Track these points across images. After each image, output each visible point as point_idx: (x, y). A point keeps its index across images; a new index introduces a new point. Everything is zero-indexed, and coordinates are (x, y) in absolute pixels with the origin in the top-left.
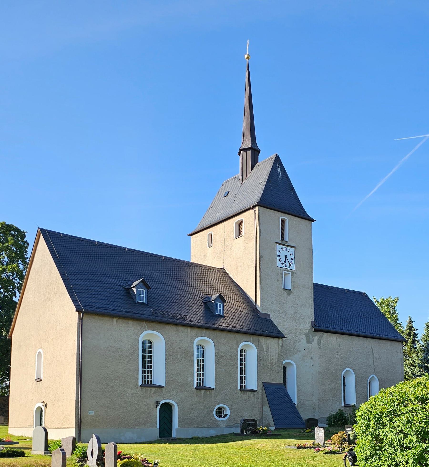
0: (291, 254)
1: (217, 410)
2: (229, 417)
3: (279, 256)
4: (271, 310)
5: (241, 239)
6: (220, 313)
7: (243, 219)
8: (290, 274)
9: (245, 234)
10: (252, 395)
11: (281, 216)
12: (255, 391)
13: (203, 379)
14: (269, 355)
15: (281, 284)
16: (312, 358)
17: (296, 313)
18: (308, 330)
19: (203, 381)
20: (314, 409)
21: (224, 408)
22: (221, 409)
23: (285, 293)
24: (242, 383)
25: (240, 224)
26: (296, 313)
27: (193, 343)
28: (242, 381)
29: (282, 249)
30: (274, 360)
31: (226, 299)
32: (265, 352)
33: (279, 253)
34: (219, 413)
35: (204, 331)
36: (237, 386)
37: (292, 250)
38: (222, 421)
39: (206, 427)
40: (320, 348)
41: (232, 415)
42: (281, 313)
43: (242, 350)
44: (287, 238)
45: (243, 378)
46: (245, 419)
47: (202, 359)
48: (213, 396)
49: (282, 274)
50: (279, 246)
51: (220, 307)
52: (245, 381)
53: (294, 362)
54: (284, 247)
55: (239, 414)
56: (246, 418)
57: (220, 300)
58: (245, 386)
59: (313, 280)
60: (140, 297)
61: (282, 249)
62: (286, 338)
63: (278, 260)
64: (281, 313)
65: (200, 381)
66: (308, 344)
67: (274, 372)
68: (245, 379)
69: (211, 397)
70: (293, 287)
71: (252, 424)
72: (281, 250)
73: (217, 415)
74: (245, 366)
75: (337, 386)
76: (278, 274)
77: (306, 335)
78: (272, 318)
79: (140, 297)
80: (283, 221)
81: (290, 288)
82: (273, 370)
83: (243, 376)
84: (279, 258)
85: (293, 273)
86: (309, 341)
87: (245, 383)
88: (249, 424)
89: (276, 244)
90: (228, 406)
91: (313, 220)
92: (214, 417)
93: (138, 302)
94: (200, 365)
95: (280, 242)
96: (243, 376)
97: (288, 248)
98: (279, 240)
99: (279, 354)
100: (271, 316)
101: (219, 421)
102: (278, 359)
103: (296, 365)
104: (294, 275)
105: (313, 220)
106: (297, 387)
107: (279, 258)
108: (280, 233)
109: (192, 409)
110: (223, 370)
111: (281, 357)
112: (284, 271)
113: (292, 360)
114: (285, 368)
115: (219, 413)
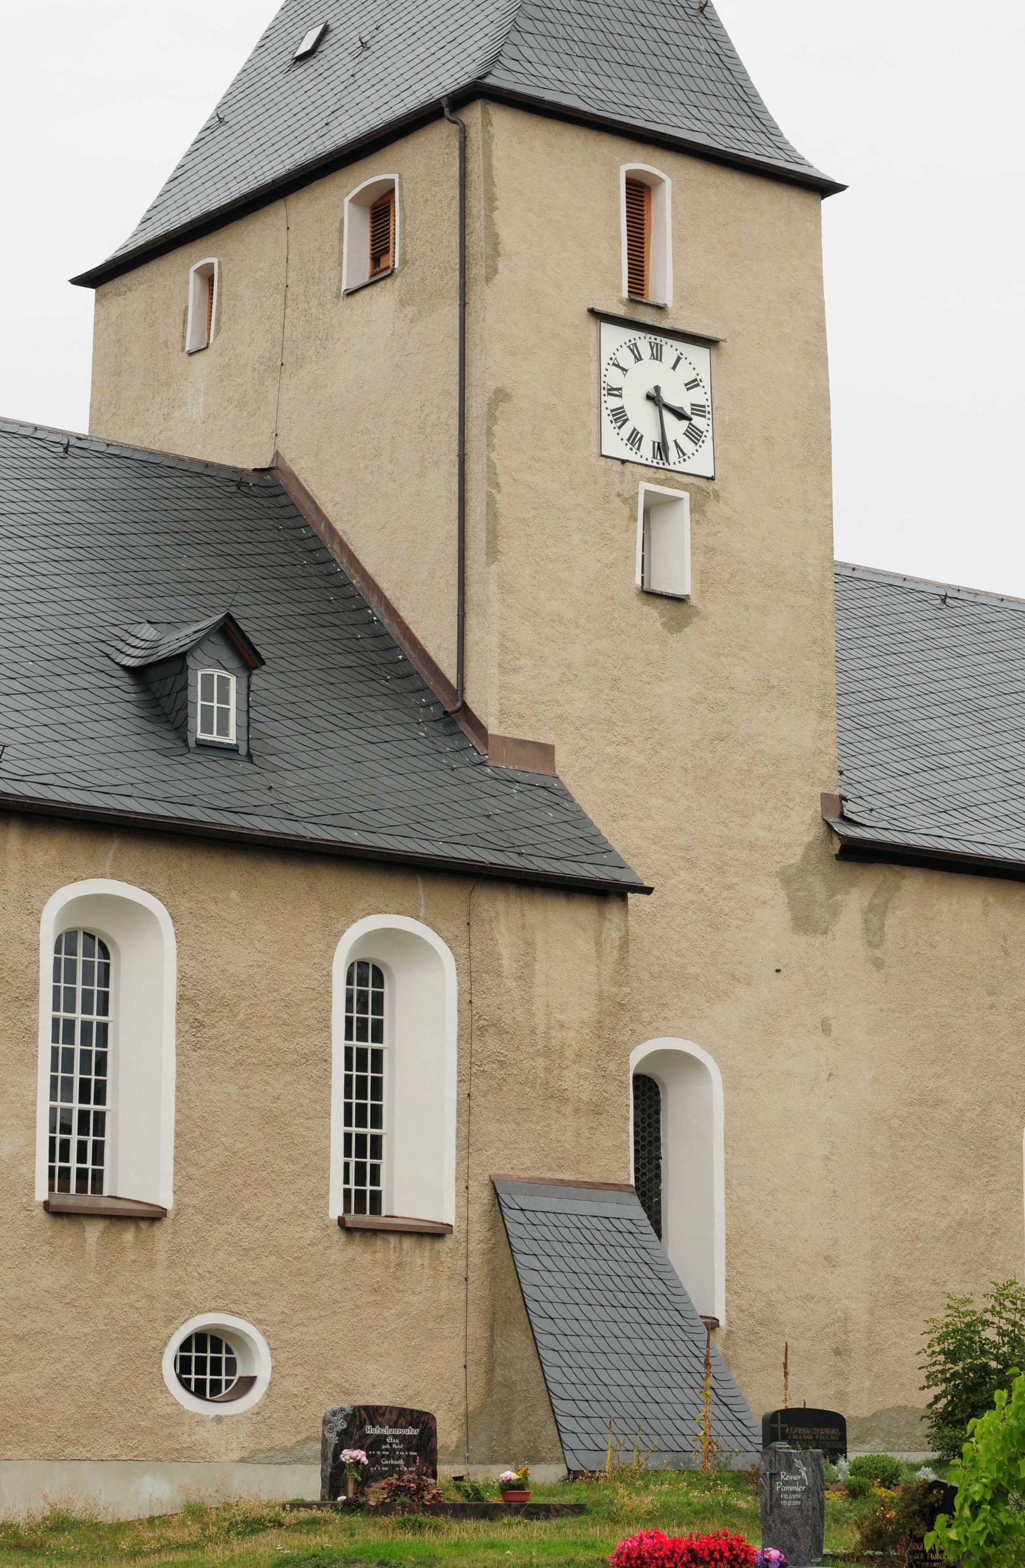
0: (692, 384)
1: (185, 1346)
2: (268, 1395)
3: (615, 392)
4: (562, 718)
5: (382, 299)
6: (223, 730)
7: (395, 177)
8: (686, 506)
9: (404, 262)
10: (418, 1256)
11: (625, 161)
12: (436, 1233)
13: (99, 1147)
14: (539, 1004)
15: (628, 558)
16: (826, 1028)
17: (720, 738)
18: (799, 851)
19: (98, 1159)
20: (837, 1352)
21: (239, 1337)
22: (217, 1347)
23: (653, 614)
24: (360, 1180)
25: (380, 209)
26: (720, 738)
27: (35, 915)
28: (360, 1167)
29: (634, 349)
30: (571, 1036)
31: (264, 654)
32: (510, 983)
33: (613, 378)
34: (201, 1370)
35: (111, 851)
36: (324, 1196)
37: (698, 357)
38: (219, 1419)
39: (115, 1458)
40: (878, 964)
41: (289, 1385)
42: (628, 740)
43: (362, 965)
44: (663, 286)
45: (365, 1150)
46: (357, 1409)
47: (95, 1018)
48: (161, 1257)
49: (630, 500)
50: (614, 337)
51: (224, 698)
52: (375, 1169)
53: (712, 1050)
54: (644, 342)
55: (334, 1375)
56: (361, 1401)
57: (224, 654)
58: (376, 1196)
59: (827, 540)
60: (207, 711)
61: (634, 349)
62: (648, 891)
63: (606, 419)
64: (628, 740)
65: (82, 1158)
66: (802, 940)
67: (568, 1109)
68: (377, 1153)
69: (151, 1265)
70: (703, 576)
71: (403, 1438)
72: (626, 358)
73: (185, 1384)
74: (378, 1067)
75: (989, 1206)
76: (606, 499)
77: (789, 878)
78: (567, 767)
79: (207, 711)
80: (639, 191)
81: (683, 587)
82: (561, 1097)
83: (369, 1131)
84: (613, 403)
85: (704, 489)
86: (805, 921)
87: (375, 1181)
88: (381, 1439)
89: (592, 324)
90: (257, 1322)
91: (825, 188)
92: (165, 1391)
93: (202, 745)
94: (86, 1055)
95: (620, 311)
96: (369, 1131)
97: (671, 348)
98: (615, 299)
99: (601, 996)
100: (561, 758)
101: (200, 1421)
102: (600, 1025)
103: (726, 1069)
104: (711, 507)
105: (825, 188)
106: (728, 1208)
107: (613, 403)
108: (617, 254)
109: (21, 1339)
110: (233, 1089)
111: (615, 1016)
112: (644, 486)
113: (696, 1039)
114: (647, 1091)
115: (201, 1370)
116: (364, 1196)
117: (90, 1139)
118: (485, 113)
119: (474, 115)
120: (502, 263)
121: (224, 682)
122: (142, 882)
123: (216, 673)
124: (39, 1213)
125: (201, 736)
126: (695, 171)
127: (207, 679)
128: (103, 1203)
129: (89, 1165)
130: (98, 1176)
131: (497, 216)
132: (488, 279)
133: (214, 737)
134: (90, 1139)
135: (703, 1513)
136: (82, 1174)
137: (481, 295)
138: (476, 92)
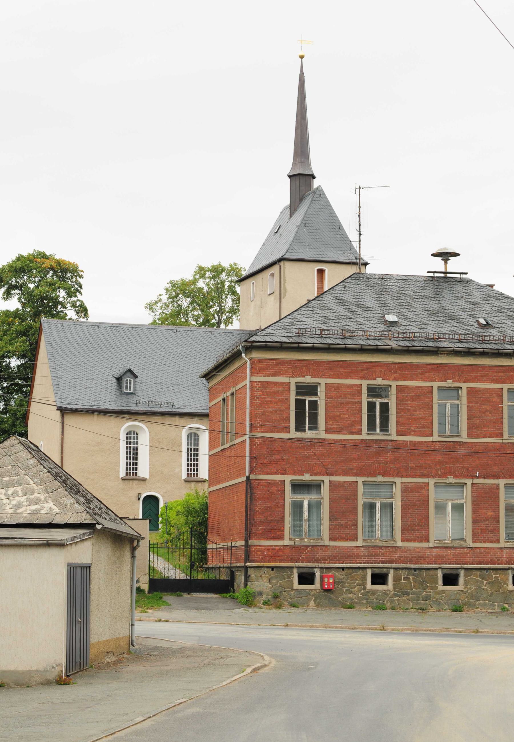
35: (195, 420)
93: (125, 393)
116: (132, 466)
117: (196, 468)
118: (284, 263)
119: (282, 263)
120: (287, 294)
121: (130, 381)
122: (139, 421)
123: (129, 379)
124: (183, 481)
125: (125, 391)
126: (333, 266)
127: (127, 380)
128: (137, 477)
129: (195, 472)
130: (197, 474)
131: (286, 284)
132: (284, 297)
133: (128, 391)
134: (196, 468)
135: (317, 499)
136: (194, 474)
137: (283, 300)
138: (280, 260)
